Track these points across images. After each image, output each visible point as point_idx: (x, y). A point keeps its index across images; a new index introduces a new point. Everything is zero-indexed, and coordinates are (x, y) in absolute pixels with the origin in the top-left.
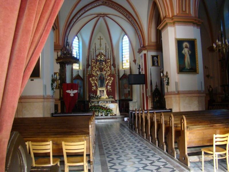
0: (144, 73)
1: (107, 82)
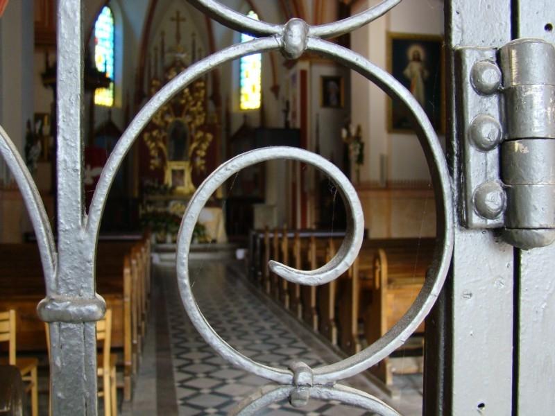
0: (298, 125)
1: (194, 145)
